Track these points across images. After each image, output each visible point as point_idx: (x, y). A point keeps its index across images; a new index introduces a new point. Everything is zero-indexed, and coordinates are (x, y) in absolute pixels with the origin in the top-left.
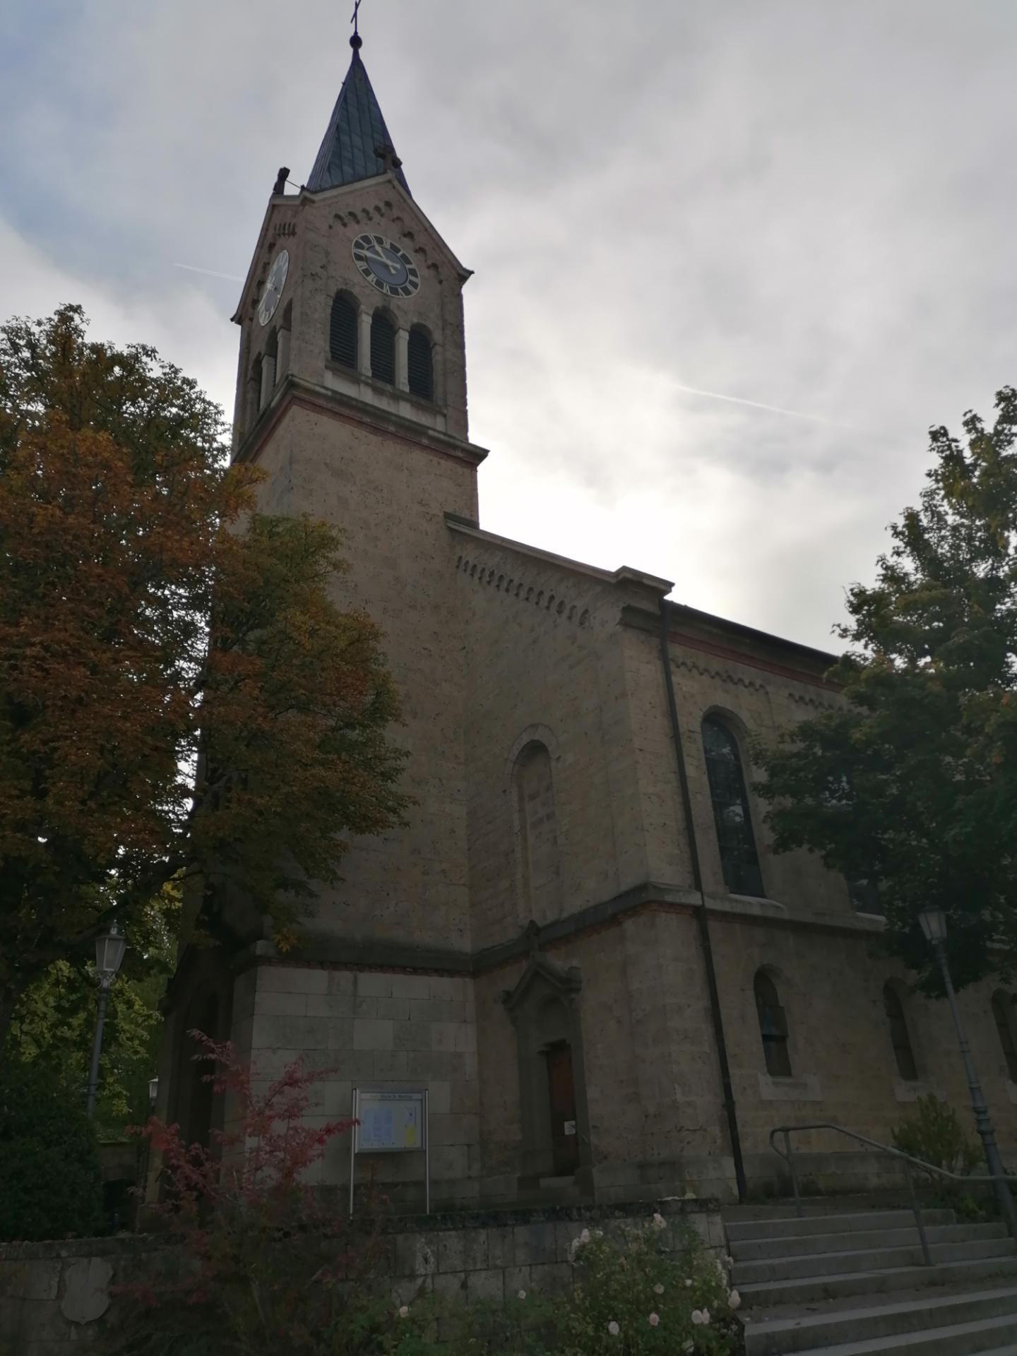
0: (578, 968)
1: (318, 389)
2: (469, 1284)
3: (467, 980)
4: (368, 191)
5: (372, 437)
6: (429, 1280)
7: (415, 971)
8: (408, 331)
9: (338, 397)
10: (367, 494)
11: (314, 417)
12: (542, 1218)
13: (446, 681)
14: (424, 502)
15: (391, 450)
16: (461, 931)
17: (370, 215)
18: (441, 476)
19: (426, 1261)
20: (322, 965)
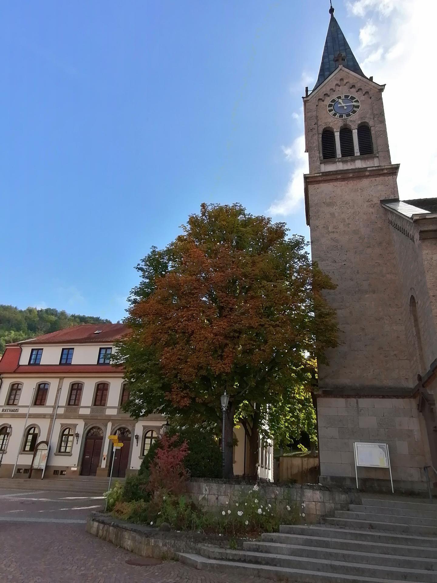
0: (432, 395)
1: (316, 175)
2: (219, 498)
3: (412, 399)
4: (341, 71)
5: (343, 183)
6: (206, 495)
7: (383, 397)
8: (356, 129)
9: (325, 174)
10: (342, 207)
11: (316, 186)
12: (245, 483)
13: (388, 274)
14: (369, 200)
15: (352, 184)
16: (407, 379)
17: (334, 89)
18: (377, 185)
19: (206, 490)
20: (342, 396)
